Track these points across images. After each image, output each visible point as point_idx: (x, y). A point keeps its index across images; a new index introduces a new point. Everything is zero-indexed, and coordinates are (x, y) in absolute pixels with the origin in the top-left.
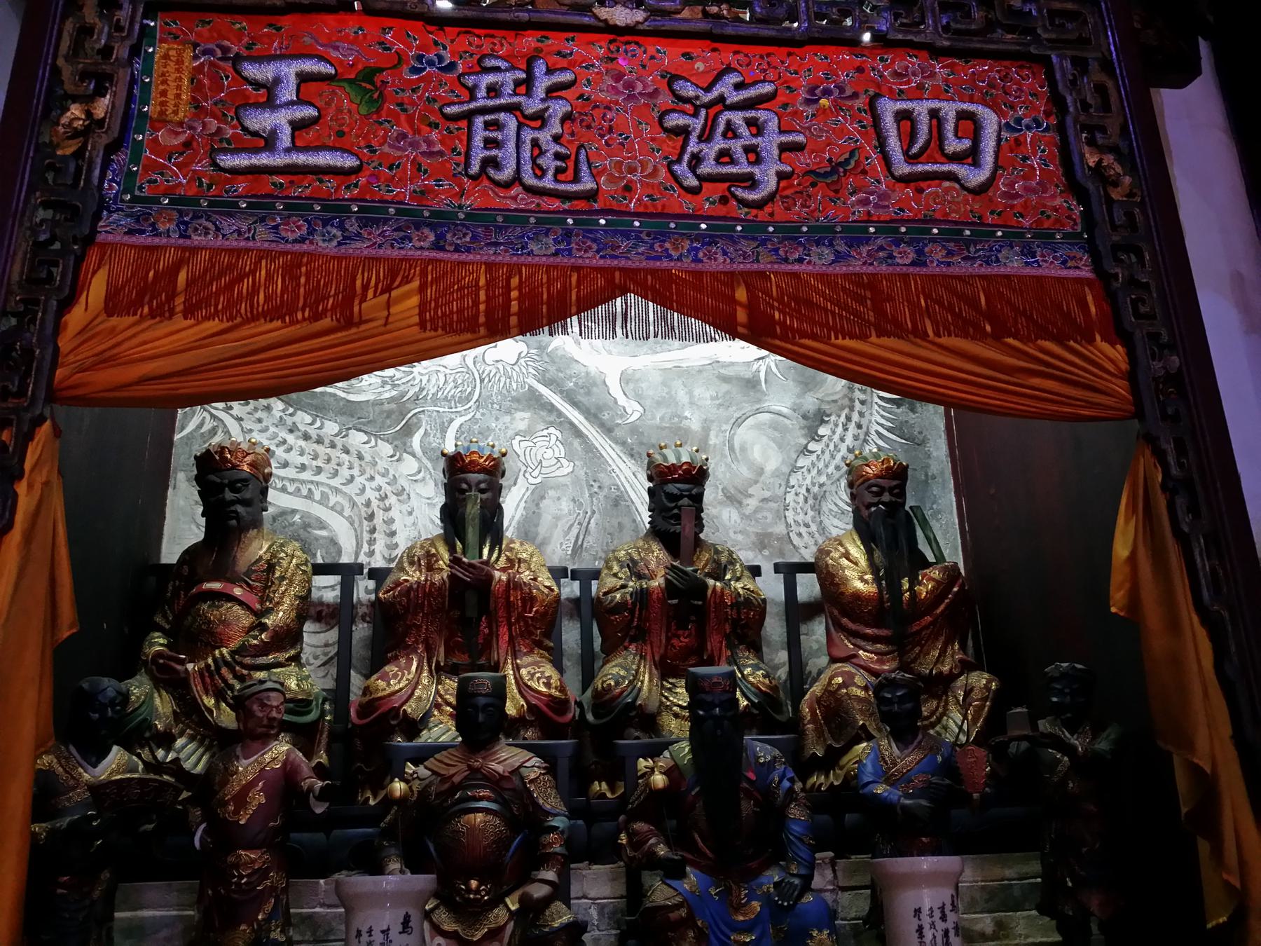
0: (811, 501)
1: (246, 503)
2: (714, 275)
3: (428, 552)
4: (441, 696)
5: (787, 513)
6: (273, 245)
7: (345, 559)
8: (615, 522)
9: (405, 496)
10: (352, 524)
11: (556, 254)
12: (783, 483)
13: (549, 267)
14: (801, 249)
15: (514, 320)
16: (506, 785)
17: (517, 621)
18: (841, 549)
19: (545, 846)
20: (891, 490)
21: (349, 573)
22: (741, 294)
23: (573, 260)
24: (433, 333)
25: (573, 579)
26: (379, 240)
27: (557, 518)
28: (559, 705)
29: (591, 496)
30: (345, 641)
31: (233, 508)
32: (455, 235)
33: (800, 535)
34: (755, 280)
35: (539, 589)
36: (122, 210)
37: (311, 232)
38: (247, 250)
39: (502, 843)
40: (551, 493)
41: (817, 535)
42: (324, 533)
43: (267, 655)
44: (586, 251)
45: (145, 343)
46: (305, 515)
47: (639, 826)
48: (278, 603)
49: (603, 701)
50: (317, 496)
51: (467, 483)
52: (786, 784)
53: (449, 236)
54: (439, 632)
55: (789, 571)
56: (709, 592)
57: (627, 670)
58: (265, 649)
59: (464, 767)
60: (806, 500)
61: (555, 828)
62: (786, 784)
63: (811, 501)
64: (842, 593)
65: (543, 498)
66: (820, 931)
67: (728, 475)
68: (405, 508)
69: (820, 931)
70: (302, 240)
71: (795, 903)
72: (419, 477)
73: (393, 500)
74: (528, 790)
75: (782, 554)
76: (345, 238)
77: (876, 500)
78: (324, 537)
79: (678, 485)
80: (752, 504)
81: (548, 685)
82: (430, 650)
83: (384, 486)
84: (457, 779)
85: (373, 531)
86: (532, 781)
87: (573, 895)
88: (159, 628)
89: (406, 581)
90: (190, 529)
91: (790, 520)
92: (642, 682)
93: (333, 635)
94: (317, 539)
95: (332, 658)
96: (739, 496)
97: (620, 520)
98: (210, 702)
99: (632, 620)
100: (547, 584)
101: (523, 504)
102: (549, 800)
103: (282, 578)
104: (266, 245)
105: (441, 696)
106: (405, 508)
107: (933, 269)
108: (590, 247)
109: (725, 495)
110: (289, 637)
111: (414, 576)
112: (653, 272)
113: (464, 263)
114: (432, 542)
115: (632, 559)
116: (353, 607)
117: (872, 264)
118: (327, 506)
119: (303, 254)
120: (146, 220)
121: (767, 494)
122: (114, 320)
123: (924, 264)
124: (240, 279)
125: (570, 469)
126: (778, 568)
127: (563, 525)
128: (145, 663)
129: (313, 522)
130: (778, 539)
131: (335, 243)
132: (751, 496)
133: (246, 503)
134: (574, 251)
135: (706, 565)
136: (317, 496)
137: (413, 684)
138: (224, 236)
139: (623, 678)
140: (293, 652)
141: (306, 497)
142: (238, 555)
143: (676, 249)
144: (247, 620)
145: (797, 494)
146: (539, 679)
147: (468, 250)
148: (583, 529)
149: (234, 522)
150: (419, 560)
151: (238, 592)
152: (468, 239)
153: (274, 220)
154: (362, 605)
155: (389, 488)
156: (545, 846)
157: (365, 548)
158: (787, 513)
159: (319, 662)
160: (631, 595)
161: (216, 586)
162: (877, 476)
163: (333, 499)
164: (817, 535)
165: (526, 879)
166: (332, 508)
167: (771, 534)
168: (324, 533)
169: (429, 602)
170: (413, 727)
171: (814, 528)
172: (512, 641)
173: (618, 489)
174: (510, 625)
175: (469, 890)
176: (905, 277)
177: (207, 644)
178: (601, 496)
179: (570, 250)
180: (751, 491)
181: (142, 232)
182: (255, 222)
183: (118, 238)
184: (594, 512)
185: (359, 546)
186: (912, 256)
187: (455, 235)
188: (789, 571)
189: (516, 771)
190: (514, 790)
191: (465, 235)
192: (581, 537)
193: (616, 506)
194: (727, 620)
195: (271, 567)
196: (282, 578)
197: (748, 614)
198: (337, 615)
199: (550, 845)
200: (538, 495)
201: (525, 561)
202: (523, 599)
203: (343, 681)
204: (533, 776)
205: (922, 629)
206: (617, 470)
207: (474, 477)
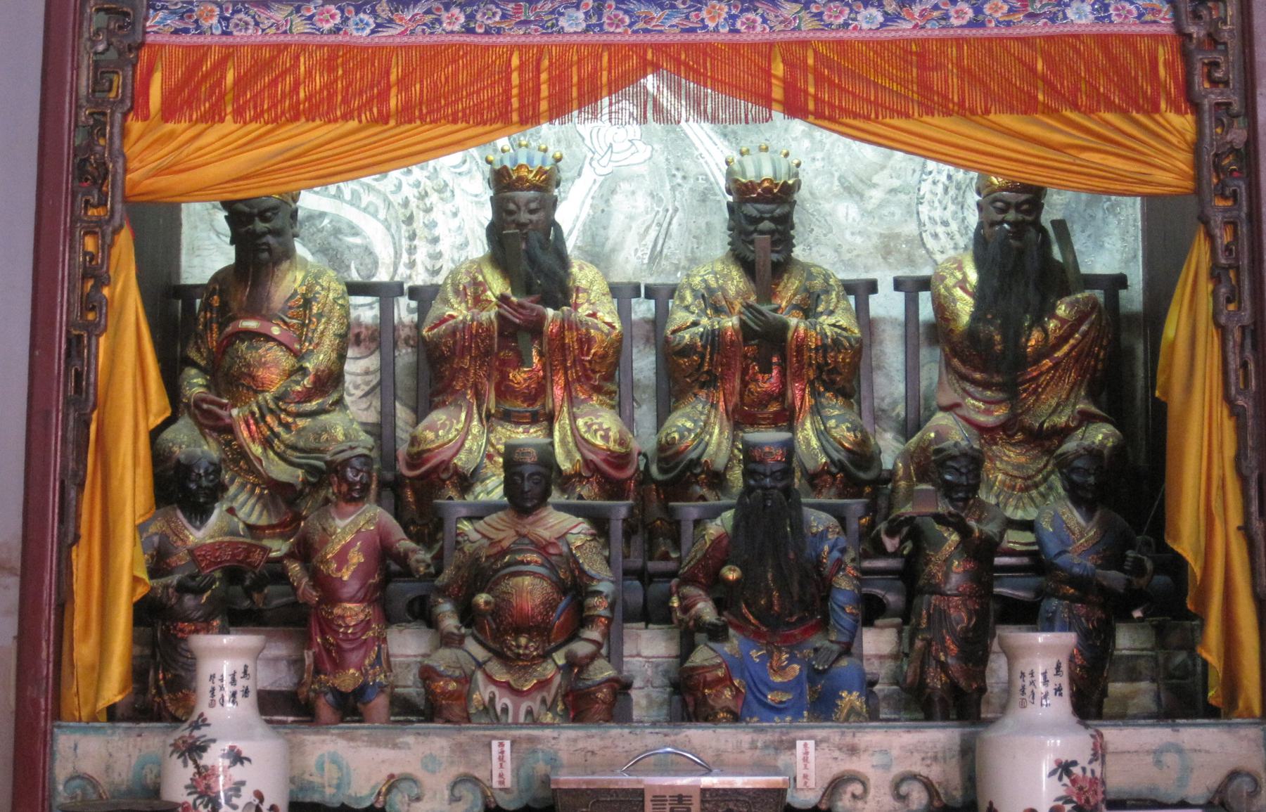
0: (952, 192)
1: (277, 233)
2: (754, 46)
3: (475, 279)
4: (493, 446)
5: (921, 208)
6: (311, 38)
7: (382, 276)
8: (702, 222)
9: (448, 194)
10: (388, 228)
11: (586, 31)
12: (918, 168)
13: (579, 45)
14: (847, 10)
15: (544, 105)
16: (552, 551)
17: (574, 362)
18: (959, 275)
19: (589, 609)
20: (1018, 207)
21: (386, 293)
22: (779, 69)
23: (604, 37)
24: (464, 125)
25: (648, 296)
26: (411, 26)
27: (631, 218)
28: (620, 460)
29: (673, 189)
30: (387, 367)
31: (264, 240)
32: (484, 14)
33: (936, 236)
34: (793, 51)
35: (597, 329)
36: (167, 8)
37: (345, 20)
38: (287, 46)
39: (550, 605)
40: (625, 186)
41: (957, 236)
42: (357, 240)
43: (310, 401)
44: (618, 26)
45: (201, 149)
46: (336, 219)
47: (690, 590)
48: (318, 344)
49: (667, 454)
50: (347, 196)
51: (515, 203)
52: (836, 554)
53: (479, 16)
54: (489, 377)
55: (911, 287)
56: (790, 334)
57: (695, 422)
58: (308, 396)
59: (512, 533)
60: (946, 190)
61: (598, 593)
62: (836, 554)
63: (952, 192)
64: (951, 331)
65: (613, 192)
66: (850, 693)
67: (847, 158)
68: (449, 208)
69: (850, 693)
70: (336, 30)
71: (830, 666)
72: (465, 168)
73: (434, 198)
74: (573, 556)
75: (911, 261)
76: (378, 25)
77: (1000, 217)
78: (357, 246)
79: (760, 206)
80: (876, 195)
81: (606, 438)
82: (479, 396)
83: (424, 181)
84: (506, 544)
85: (412, 237)
86: (577, 548)
87: (626, 652)
88: (194, 364)
89: (452, 317)
90: (210, 239)
91: (924, 217)
92: (711, 436)
93: (373, 362)
94: (349, 248)
95: (373, 389)
96: (860, 186)
97: (708, 219)
98: (257, 449)
99: (701, 365)
100: (608, 319)
101: (589, 201)
102: (594, 564)
103: (320, 315)
104: (303, 38)
105: (493, 446)
106: (449, 208)
107: (992, 30)
108: (622, 21)
109: (842, 184)
110: (330, 380)
111: (459, 311)
112: (687, 46)
113: (494, 46)
114: (479, 263)
115: (708, 288)
116: (394, 328)
117: (923, 28)
118: (358, 207)
119: (339, 46)
120: (190, 17)
121: (896, 183)
122: (170, 126)
123: (982, 25)
124: (284, 74)
125: (648, 155)
126: (898, 284)
127: (637, 227)
128: (188, 406)
129: (344, 227)
130: (907, 242)
131: (368, 31)
132: (875, 186)
133: (277, 233)
134: (606, 27)
135: (795, 295)
136: (347, 196)
137: (460, 433)
138: (263, 30)
139: (689, 430)
140: (335, 396)
141: (334, 196)
142: (273, 290)
143: (713, 18)
144: (287, 362)
145: (934, 183)
146: (596, 431)
147: (499, 32)
148: (663, 231)
149: (265, 255)
150: (465, 288)
151: (276, 331)
152: (497, 18)
153: (309, 10)
154: (404, 326)
155: (429, 183)
156: (589, 609)
157: (405, 258)
158: (921, 208)
159: (359, 393)
160: (702, 336)
161: (252, 324)
162: (1001, 189)
163: (366, 199)
164: (957, 236)
165: (574, 636)
166: (365, 210)
167: (898, 236)
168: (357, 240)
169: (477, 343)
170: (466, 482)
171: (954, 226)
172: (567, 387)
173: (707, 180)
174: (566, 369)
175: (519, 647)
176: (959, 41)
177: (249, 388)
178: (686, 187)
179: (601, 25)
180: (875, 179)
181: (186, 31)
182: (291, 14)
183: (166, 38)
184: (676, 210)
185: (397, 255)
186: (970, 14)
187: (484, 14)
188: (911, 287)
189: (562, 537)
190: (560, 555)
191: (494, 14)
192: (660, 242)
193: (704, 201)
194: (810, 365)
195: (307, 303)
196: (320, 315)
197: (836, 357)
198: (380, 337)
199: (595, 607)
200: (608, 189)
201: (585, 291)
202: (580, 341)
203: (387, 415)
204: (579, 543)
205: (1041, 374)
206: (705, 154)
207: (524, 195)
